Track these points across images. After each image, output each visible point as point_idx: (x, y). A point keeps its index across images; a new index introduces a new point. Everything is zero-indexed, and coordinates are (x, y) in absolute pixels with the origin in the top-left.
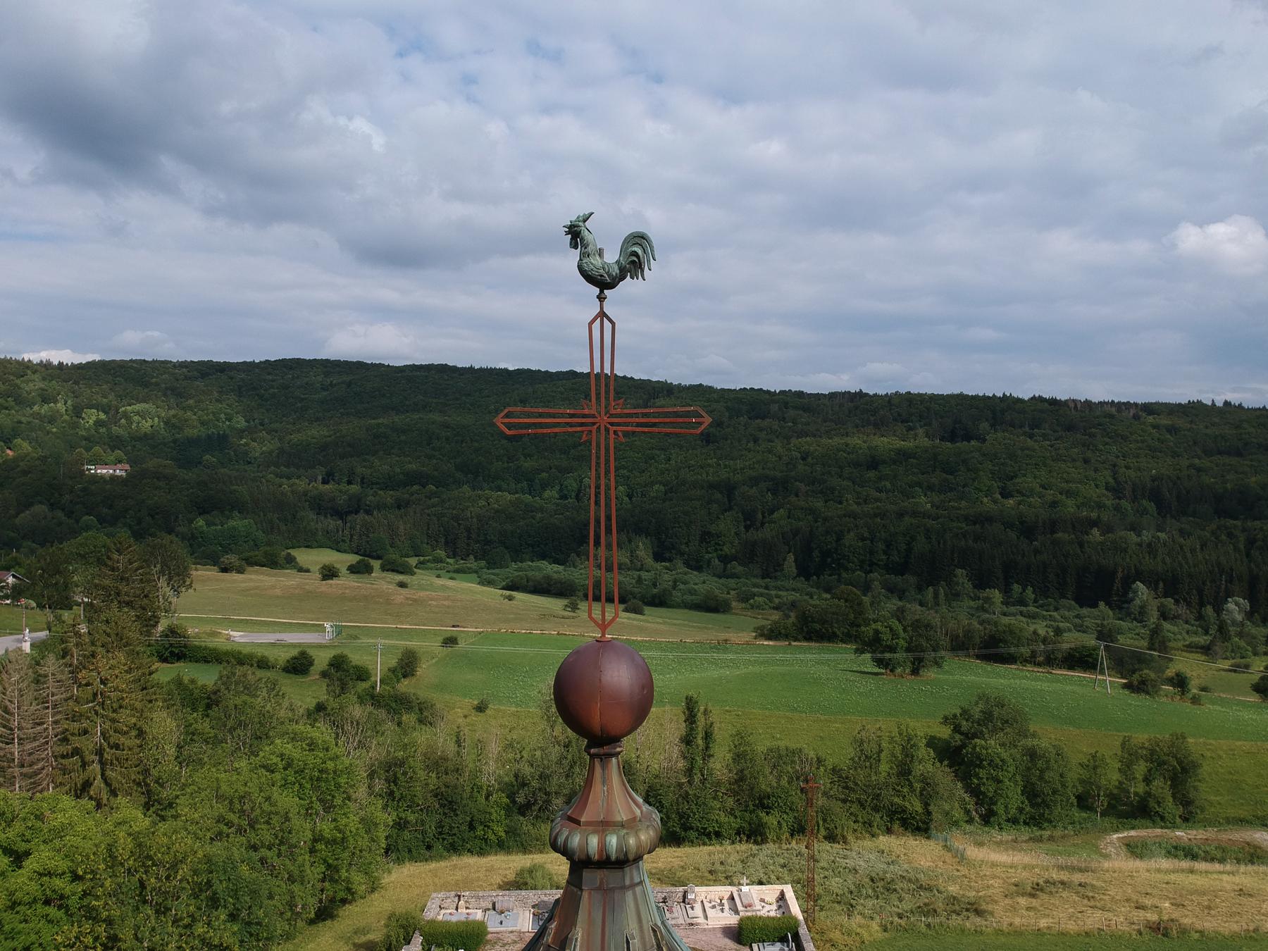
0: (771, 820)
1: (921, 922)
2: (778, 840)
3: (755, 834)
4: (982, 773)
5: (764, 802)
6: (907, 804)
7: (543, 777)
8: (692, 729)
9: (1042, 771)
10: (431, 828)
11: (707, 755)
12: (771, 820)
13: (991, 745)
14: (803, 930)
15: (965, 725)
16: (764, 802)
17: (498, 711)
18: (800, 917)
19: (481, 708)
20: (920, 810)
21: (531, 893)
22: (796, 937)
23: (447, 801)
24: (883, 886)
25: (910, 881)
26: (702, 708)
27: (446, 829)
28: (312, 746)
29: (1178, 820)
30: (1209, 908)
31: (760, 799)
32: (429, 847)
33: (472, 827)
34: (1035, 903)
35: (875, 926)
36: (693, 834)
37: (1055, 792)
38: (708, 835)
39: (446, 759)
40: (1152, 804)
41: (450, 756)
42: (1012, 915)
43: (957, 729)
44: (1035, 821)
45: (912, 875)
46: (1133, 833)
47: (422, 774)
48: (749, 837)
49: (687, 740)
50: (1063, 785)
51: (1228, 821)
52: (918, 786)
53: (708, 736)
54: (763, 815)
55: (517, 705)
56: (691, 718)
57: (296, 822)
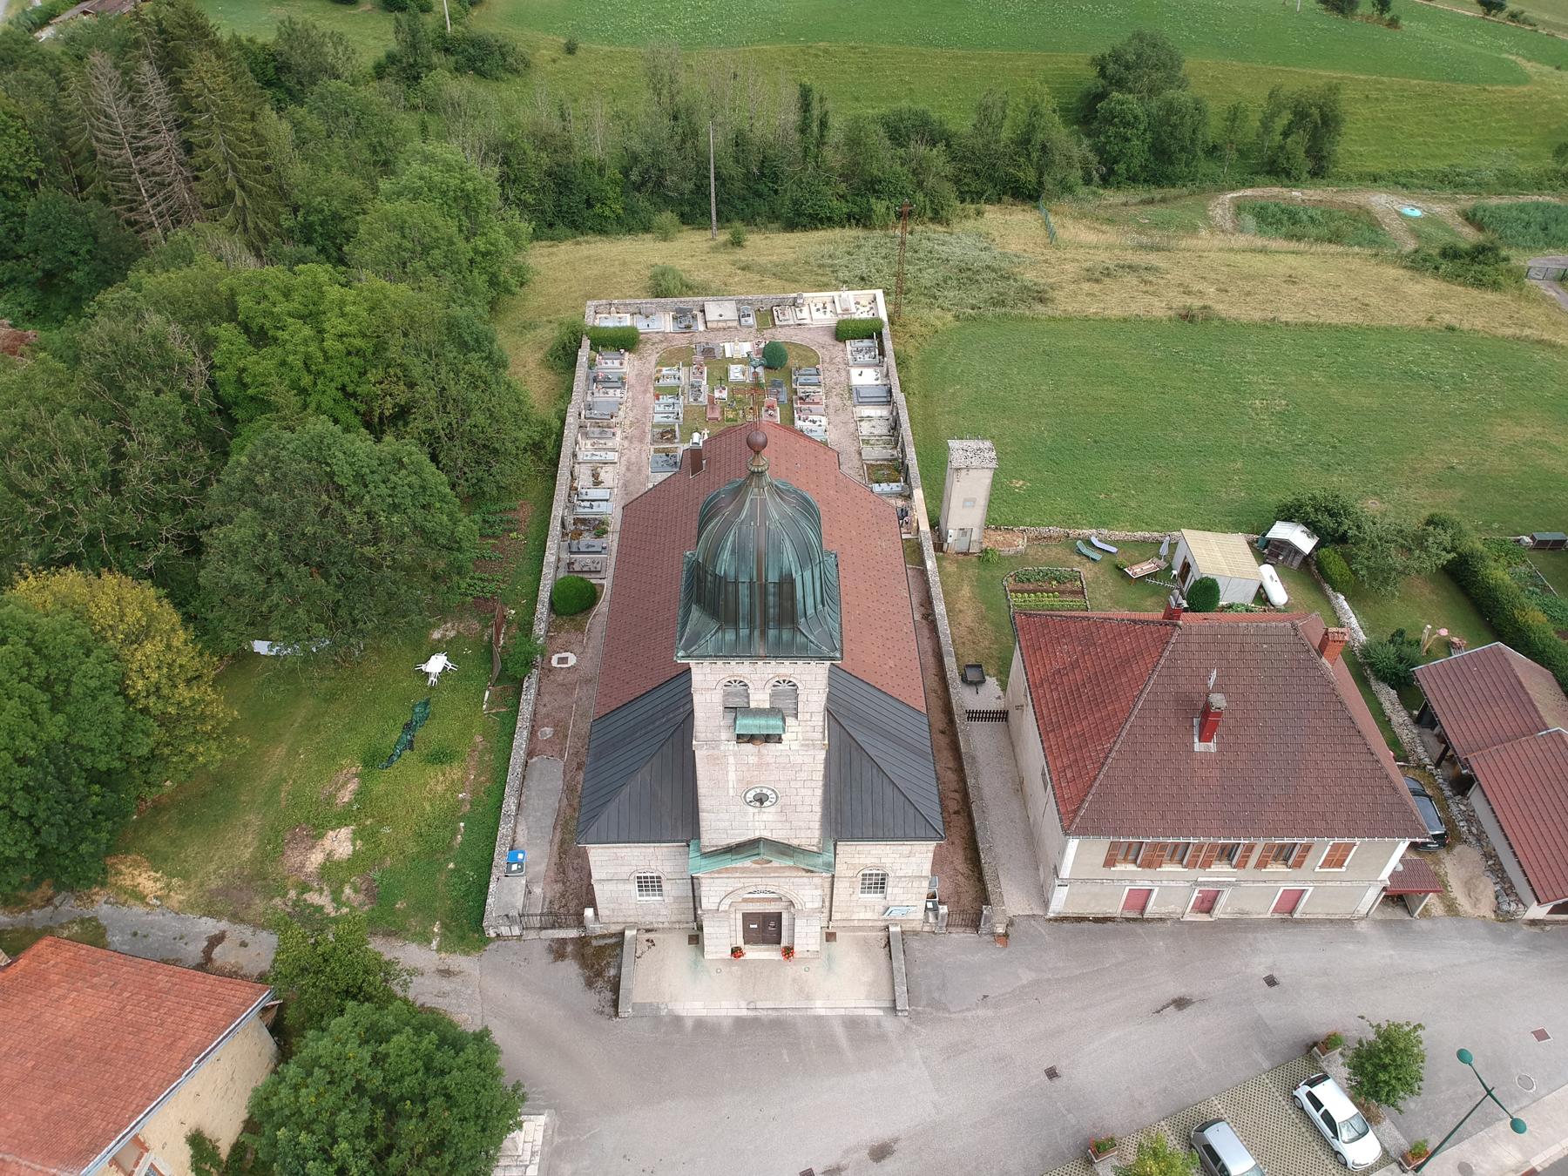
0: (879, 207)
1: (990, 313)
2: (885, 227)
3: (862, 219)
4: (1112, 130)
5: (873, 187)
6: (1021, 174)
7: (656, 154)
8: (806, 118)
9: (1174, 126)
10: (548, 205)
11: (821, 143)
12: (879, 207)
13: (1125, 101)
14: (886, 331)
15: (1111, 68)
16: (873, 187)
17: (589, 51)
18: (885, 319)
19: (571, 49)
20: (1034, 180)
21: (669, 300)
22: (880, 335)
23: (561, 181)
24: (967, 275)
25: (994, 270)
26: (817, 97)
27: (565, 208)
28: (449, 168)
29: (1305, 175)
30: (1248, 294)
31: (872, 182)
32: (551, 225)
33: (589, 205)
34: (1097, 287)
35: (949, 317)
36: (805, 220)
37: (1183, 149)
38: (821, 221)
39: (553, 136)
40: (1282, 160)
41: (558, 131)
42: (1075, 301)
43: (1102, 73)
44: (1157, 178)
45: (995, 265)
46: (1249, 192)
47: (532, 154)
48: (858, 221)
49: (803, 129)
50: (1192, 141)
51: (1361, 177)
52: (1035, 155)
53: (823, 124)
54: (873, 200)
55: (611, 43)
56: (805, 107)
57: (461, 244)
